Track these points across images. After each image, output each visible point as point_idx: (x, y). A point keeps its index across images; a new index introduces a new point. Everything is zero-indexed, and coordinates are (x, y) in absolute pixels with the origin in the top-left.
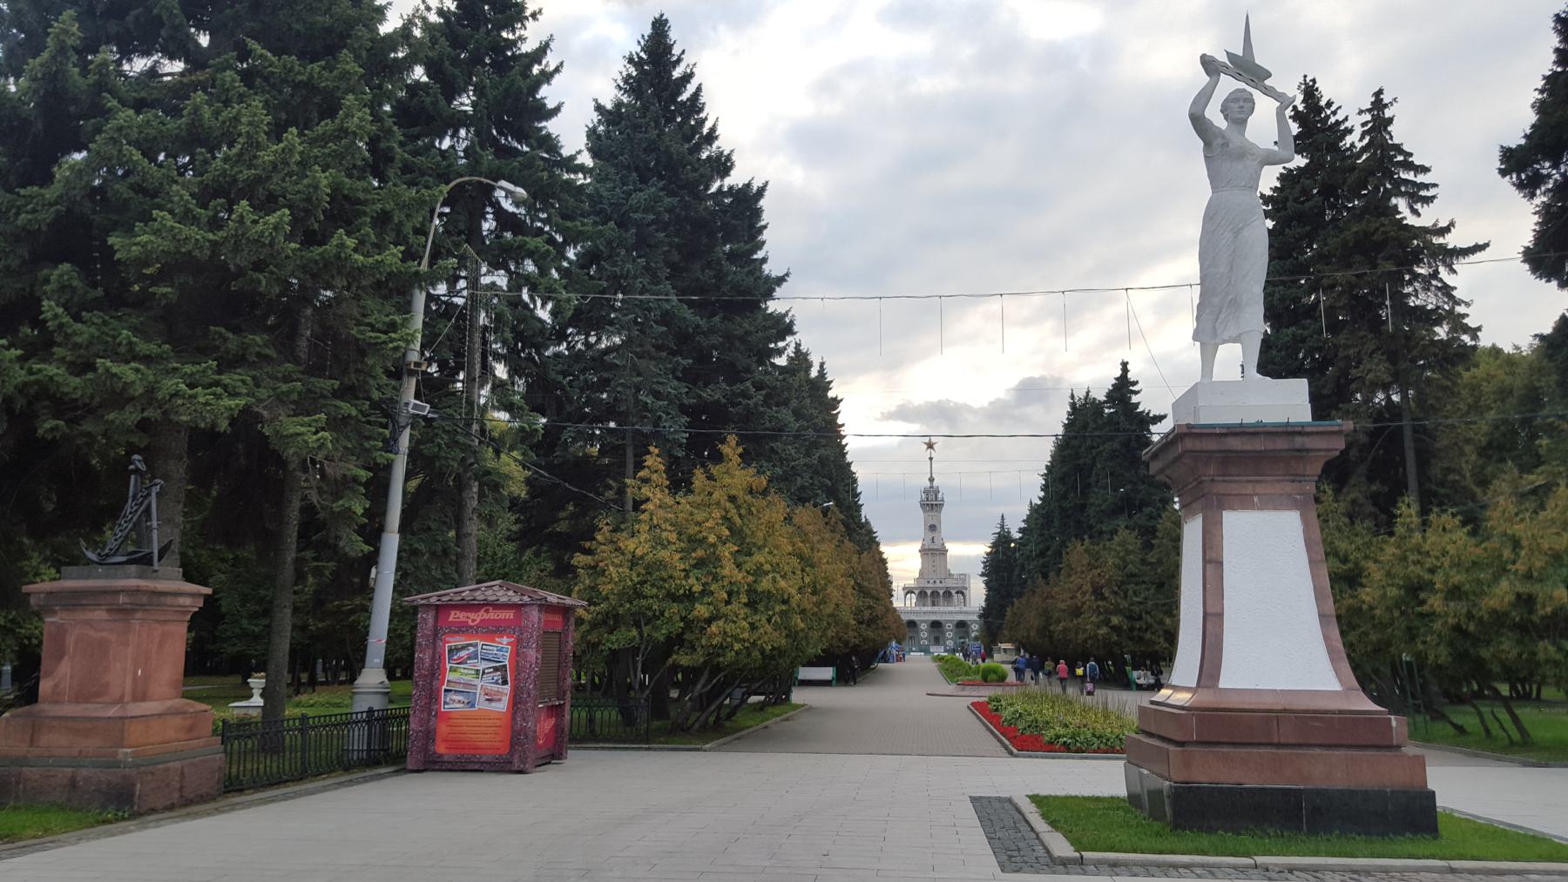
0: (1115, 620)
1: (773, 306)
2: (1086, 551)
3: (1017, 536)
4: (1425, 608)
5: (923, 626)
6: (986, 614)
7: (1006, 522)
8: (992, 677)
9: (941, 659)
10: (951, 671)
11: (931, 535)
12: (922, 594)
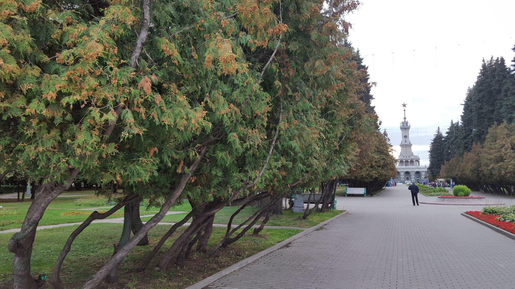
1: (445, 135)
2: (506, 127)
4: (283, 160)
6: (431, 168)
11: (405, 139)
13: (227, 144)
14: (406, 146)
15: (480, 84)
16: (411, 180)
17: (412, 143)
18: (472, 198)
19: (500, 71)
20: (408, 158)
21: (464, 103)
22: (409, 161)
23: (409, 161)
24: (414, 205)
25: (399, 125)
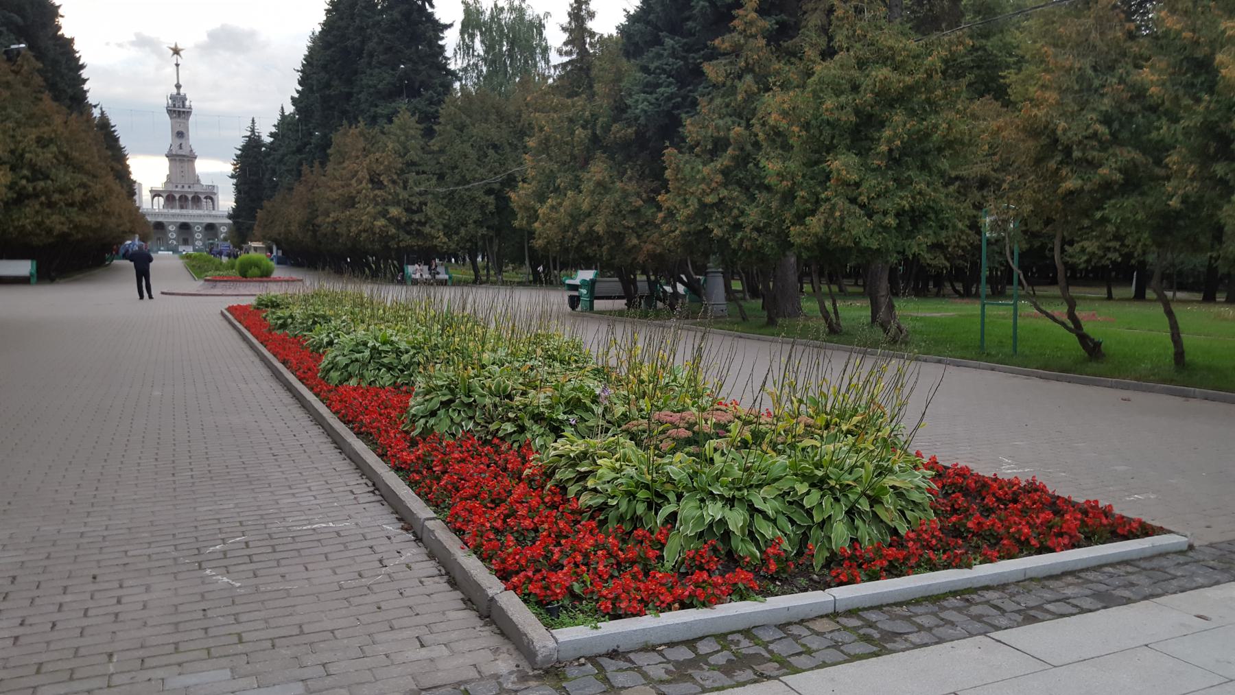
0: (394, 211)
1: (268, 140)
2: (362, 134)
3: (269, 140)
5: (172, 228)
6: (235, 215)
7: (257, 126)
8: (248, 273)
9: (188, 257)
10: (196, 267)
11: (178, 141)
12: (170, 199)
13: (421, 113)
14: (181, 158)
15: (328, 26)
16: (194, 245)
17: (196, 151)
18: (276, 281)
19: (365, 8)
20: (186, 189)
21: (299, 67)
22: (190, 197)
23: (190, 197)
24: (142, 297)
25: (164, 102)
